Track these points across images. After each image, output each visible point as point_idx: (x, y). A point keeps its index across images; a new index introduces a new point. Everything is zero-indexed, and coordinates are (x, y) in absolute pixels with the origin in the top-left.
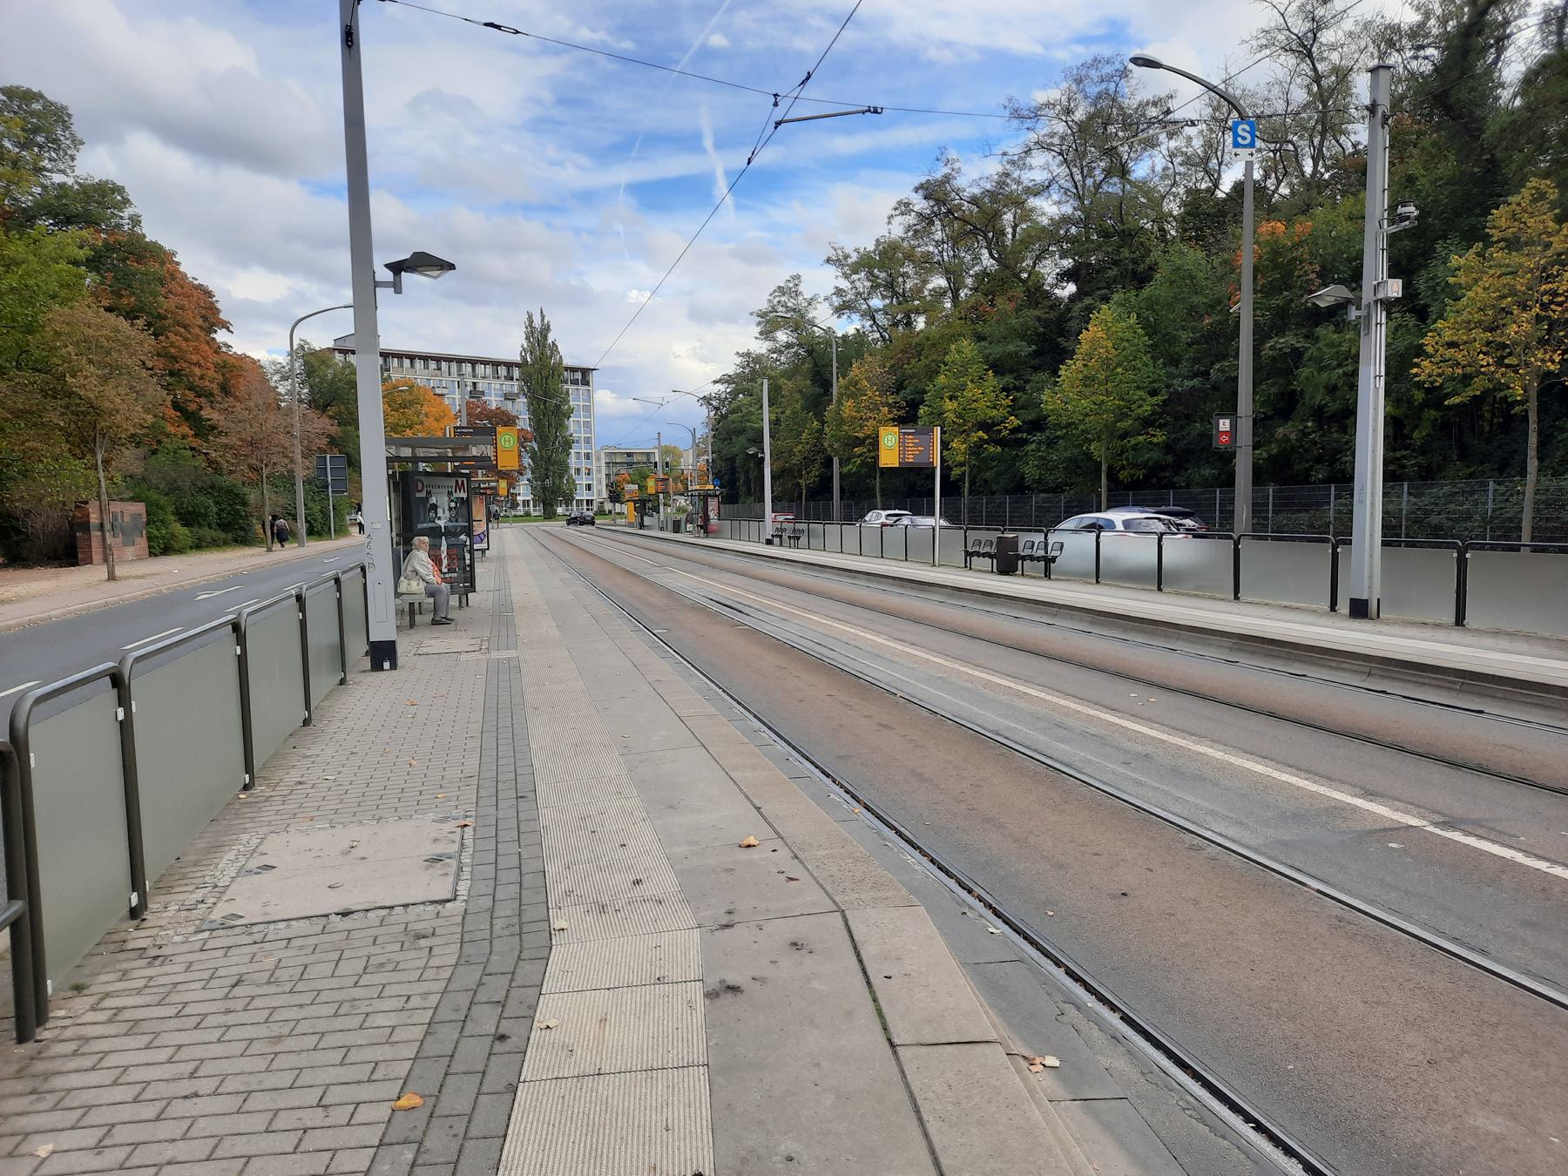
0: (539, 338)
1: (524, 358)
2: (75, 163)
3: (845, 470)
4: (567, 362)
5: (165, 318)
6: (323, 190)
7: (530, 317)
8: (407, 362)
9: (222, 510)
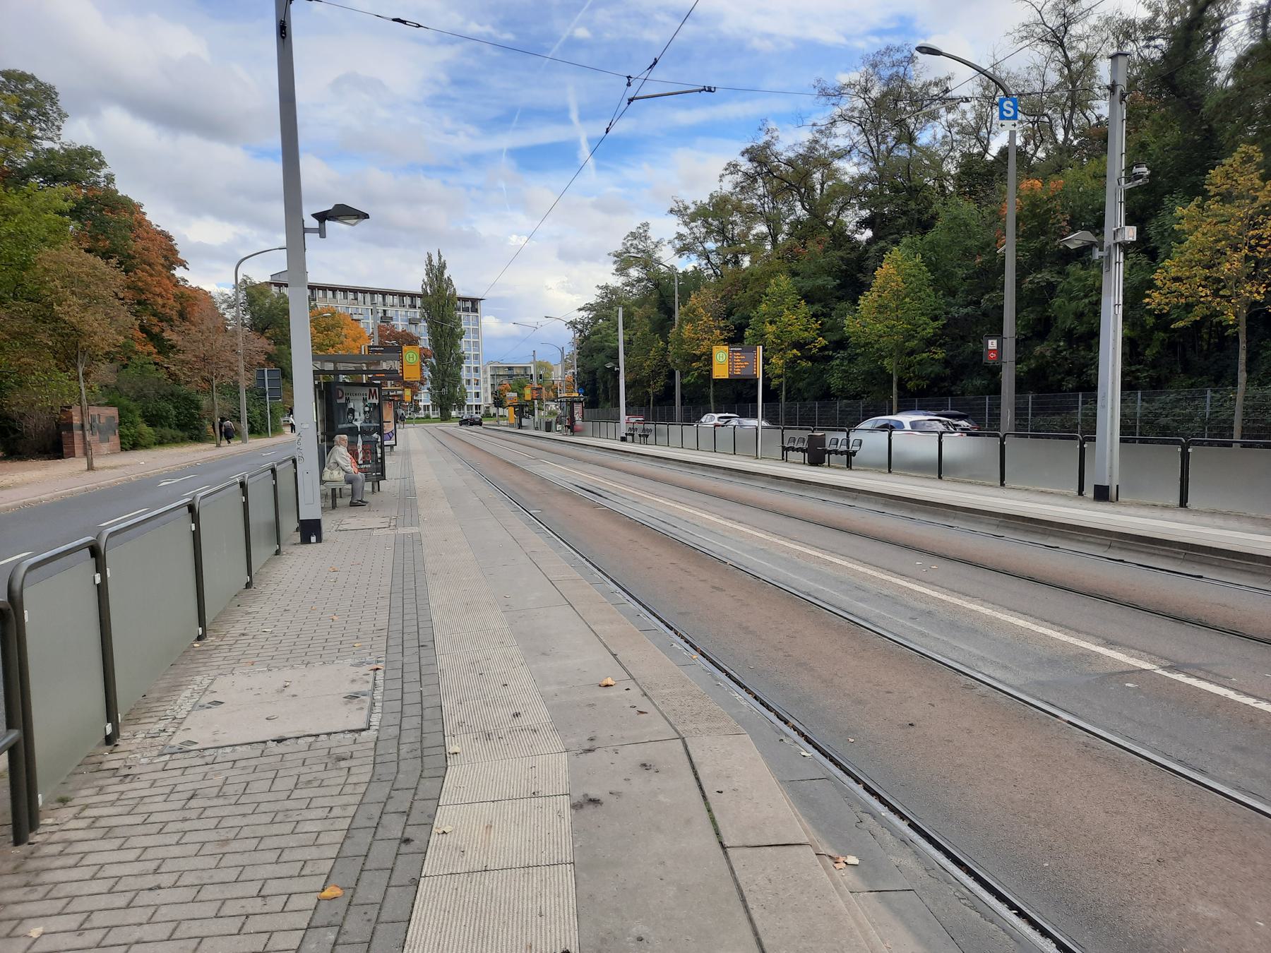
0: (437, 274)
1: (425, 290)
2: (61, 132)
3: (685, 381)
4: (460, 293)
5: (134, 258)
6: (262, 154)
7: (430, 257)
8: (330, 294)
9: (180, 413)
